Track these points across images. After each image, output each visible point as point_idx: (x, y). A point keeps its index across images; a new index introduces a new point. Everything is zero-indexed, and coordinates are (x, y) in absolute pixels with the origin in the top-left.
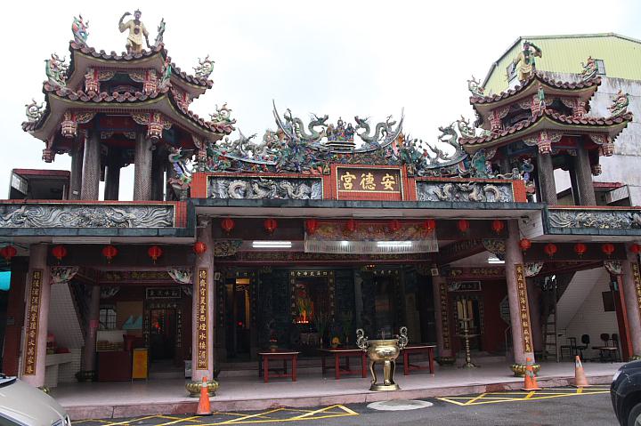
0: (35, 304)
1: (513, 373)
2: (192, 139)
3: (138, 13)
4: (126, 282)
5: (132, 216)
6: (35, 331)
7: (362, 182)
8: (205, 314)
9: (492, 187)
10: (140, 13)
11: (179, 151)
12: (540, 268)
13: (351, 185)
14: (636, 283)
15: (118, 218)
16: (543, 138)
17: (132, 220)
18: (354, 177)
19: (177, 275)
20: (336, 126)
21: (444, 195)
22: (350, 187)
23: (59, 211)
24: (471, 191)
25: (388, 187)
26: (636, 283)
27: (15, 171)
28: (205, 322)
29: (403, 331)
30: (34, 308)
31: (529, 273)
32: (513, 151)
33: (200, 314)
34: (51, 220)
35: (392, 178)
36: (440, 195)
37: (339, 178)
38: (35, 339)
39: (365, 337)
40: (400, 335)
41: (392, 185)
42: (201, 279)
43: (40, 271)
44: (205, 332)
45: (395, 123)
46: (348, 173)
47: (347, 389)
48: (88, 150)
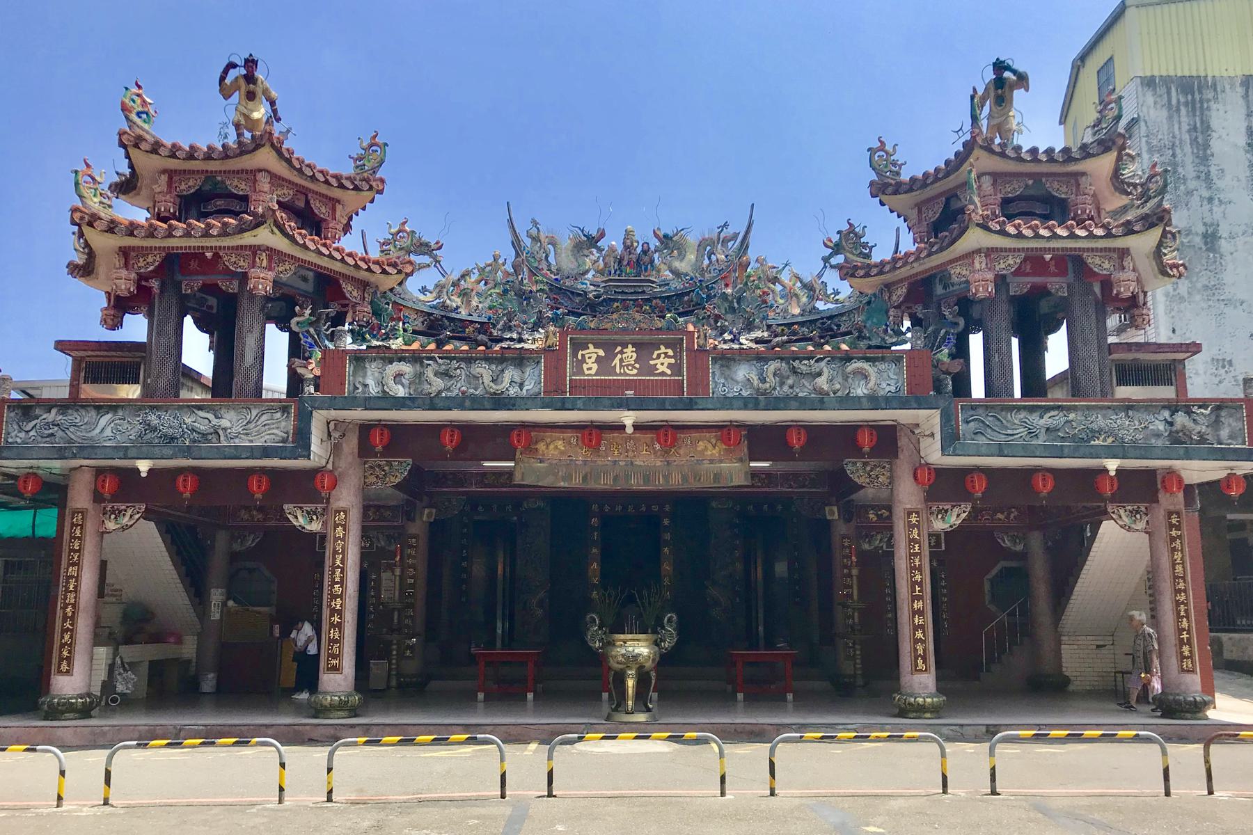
0: (74, 564)
1: (897, 711)
2: (340, 286)
3: (251, 63)
4: (272, 523)
5: (225, 423)
6: (74, 606)
7: (617, 361)
8: (341, 583)
9: (859, 364)
10: (255, 62)
11: (308, 312)
12: (964, 515)
13: (595, 367)
14: (1174, 549)
15: (203, 427)
16: (977, 266)
17: (225, 429)
18: (601, 353)
19: (300, 518)
20: (620, 249)
21: (763, 381)
22: (593, 372)
23: (109, 416)
24: (819, 374)
25: (661, 369)
26: (1174, 549)
27: (62, 346)
28: (341, 596)
29: (670, 620)
30: (72, 571)
31: (939, 525)
32: (945, 288)
33: (333, 583)
34: (97, 431)
35: (670, 352)
36: (756, 382)
37: (575, 354)
38: (73, 618)
39: (600, 628)
40: (663, 628)
41: (670, 366)
42: (336, 526)
43: (83, 512)
44: (340, 613)
45: (736, 236)
46: (591, 346)
47: (566, 717)
48: (160, 315)
